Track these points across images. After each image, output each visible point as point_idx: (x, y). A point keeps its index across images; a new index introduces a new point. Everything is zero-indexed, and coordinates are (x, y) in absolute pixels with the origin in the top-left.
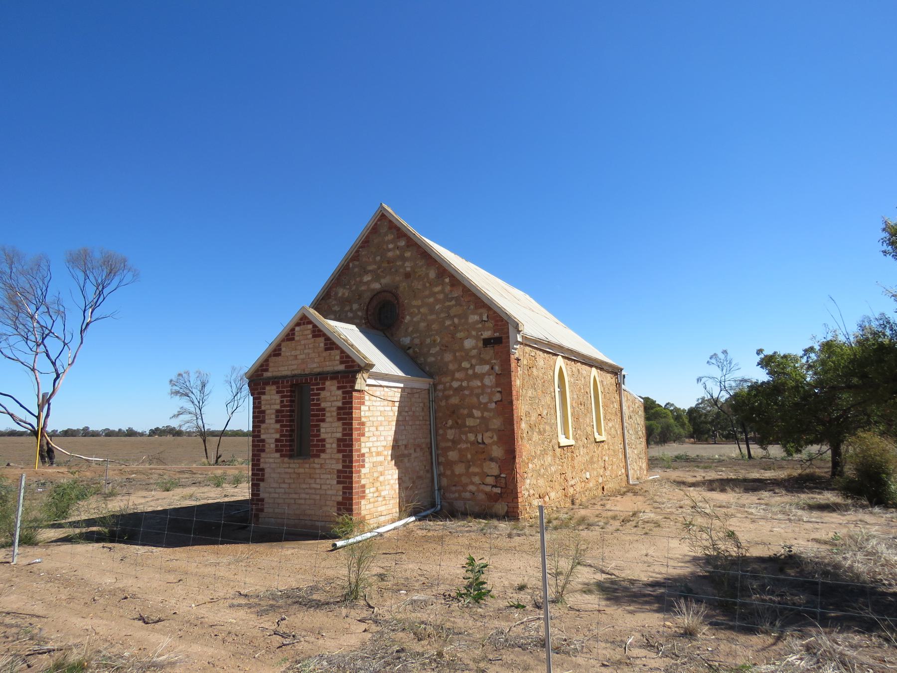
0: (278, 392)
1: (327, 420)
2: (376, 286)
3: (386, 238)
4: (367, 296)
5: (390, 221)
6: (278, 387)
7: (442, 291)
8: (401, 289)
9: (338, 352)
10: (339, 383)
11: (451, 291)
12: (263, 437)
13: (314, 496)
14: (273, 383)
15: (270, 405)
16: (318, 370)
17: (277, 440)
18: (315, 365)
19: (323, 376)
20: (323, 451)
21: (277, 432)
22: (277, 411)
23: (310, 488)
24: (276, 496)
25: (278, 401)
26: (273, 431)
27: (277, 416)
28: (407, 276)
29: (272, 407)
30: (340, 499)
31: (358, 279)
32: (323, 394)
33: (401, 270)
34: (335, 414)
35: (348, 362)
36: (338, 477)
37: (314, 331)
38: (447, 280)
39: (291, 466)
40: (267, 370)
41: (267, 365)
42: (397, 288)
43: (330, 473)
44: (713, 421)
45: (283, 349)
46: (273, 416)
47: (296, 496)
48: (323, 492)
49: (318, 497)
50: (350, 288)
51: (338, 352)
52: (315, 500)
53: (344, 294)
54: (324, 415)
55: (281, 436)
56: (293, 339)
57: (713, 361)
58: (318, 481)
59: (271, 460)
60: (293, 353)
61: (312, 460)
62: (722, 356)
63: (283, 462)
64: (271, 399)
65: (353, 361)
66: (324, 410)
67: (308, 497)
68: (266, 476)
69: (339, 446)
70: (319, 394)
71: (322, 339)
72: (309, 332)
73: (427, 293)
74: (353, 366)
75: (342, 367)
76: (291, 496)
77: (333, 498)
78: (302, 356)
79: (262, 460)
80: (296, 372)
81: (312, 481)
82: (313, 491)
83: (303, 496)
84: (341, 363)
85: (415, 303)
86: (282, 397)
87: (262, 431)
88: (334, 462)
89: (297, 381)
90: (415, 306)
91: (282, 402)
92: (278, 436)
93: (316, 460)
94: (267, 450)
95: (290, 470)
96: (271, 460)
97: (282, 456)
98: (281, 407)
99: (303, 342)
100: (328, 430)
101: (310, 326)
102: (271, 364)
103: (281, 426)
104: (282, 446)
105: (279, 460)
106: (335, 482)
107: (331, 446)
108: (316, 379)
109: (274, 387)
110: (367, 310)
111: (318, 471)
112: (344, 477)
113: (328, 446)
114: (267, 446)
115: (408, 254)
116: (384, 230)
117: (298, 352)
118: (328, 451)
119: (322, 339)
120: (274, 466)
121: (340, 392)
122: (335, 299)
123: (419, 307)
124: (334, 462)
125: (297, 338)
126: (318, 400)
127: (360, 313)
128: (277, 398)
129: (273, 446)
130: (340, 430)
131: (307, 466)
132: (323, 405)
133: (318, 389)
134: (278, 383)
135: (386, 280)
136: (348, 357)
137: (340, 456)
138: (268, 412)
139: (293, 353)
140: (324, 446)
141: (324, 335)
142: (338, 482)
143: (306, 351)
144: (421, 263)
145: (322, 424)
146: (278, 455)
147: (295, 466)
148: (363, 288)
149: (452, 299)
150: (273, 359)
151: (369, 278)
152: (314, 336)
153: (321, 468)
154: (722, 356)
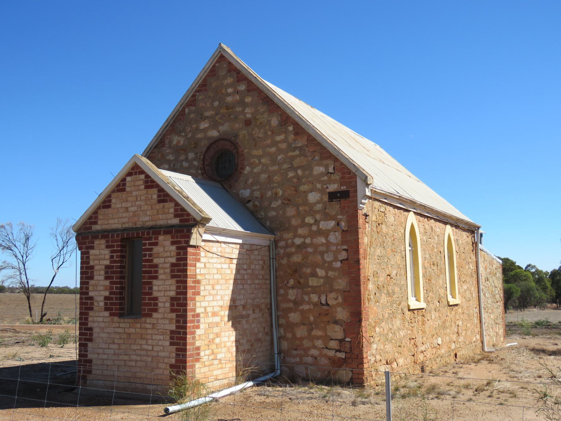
0: (107, 247)
1: (161, 277)
2: (214, 134)
3: (226, 82)
4: (204, 144)
6: (107, 242)
7: (285, 141)
10: (172, 237)
11: (295, 140)
13: (145, 358)
14: (103, 237)
16: (151, 224)
17: (106, 298)
18: (147, 218)
20: (156, 310)
21: (106, 290)
22: (107, 267)
23: (141, 350)
24: (105, 357)
25: (108, 257)
26: (102, 288)
27: (106, 273)
28: (248, 123)
29: (102, 262)
30: (173, 361)
34: (168, 271)
36: (172, 338)
37: (146, 182)
38: (291, 128)
39: (121, 325)
40: (96, 223)
41: (96, 218)
42: (236, 136)
43: (163, 334)
45: (114, 201)
46: (102, 272)
47: (126, 358)
48: (155, 354)
49: (149, 359)
50: (186, 136)
51: (172, 204)
53: (179, 142)
54: (156, 272)
55: (111, 293)
56: (124, 190)
58: (150, 342)
59: (100, 319)
60: (124, 205)
63: (113, 322)
64: (100, 254)
65: (189, 215)
66: (156, 266)
67: (139, 358)
68: (95, 335)
70: (151, 250)
71: (155, 190)
72: (141, 182)
73: (269, 142)
74: (188, 220)
75: (176, 221)
76: (121, 357)
77: (166, 360)
80: (127, 226)
81: (144, 342)
82: (144, 353)
84: (176, 216)
85: (255, 152)
86: (112, 252)
87: (91, 288)
88: (167, 322)
89: (128, 234)
90: (255, 156)
91: (112, 257)
92: (107, 293)
93: (148, 320)
94: (95, 308)
95: (120, 330)
96: (100, 319)
97: (111, 315)
98: (111, 262)
99: (134, 193)
100: (161, 288)
101: (142, 177)
106: (168, 343)
107: (164, 305)
109: (103, 241)
111: (149, 332)
115: (248, 100)
116: (222, 73)
119: (155, 190)
120: (102, 325)
122: (170, 147)
123: (259, 157)
125: (128, 189)
126: (150, 255)
127: (196, 163)
128: (107, 253)
129: (102, 304)
130: (174, 288)
131: (138, 326)
133: (150, 244)
135: (225, 128)
136: (183, 209)
137: (174, 315)
138: (96, 268)
139: (124, 205)
140: (156, 305)
141: (158, 186)
142: (172, 344)
143: (138, 203)
144: (262, 109)
145: (155, 282)
146: (107, 314)
147: (125, 325)
148: (200, 136)
149: (296, 148)
150: (102, 211)
153: (153, 328)
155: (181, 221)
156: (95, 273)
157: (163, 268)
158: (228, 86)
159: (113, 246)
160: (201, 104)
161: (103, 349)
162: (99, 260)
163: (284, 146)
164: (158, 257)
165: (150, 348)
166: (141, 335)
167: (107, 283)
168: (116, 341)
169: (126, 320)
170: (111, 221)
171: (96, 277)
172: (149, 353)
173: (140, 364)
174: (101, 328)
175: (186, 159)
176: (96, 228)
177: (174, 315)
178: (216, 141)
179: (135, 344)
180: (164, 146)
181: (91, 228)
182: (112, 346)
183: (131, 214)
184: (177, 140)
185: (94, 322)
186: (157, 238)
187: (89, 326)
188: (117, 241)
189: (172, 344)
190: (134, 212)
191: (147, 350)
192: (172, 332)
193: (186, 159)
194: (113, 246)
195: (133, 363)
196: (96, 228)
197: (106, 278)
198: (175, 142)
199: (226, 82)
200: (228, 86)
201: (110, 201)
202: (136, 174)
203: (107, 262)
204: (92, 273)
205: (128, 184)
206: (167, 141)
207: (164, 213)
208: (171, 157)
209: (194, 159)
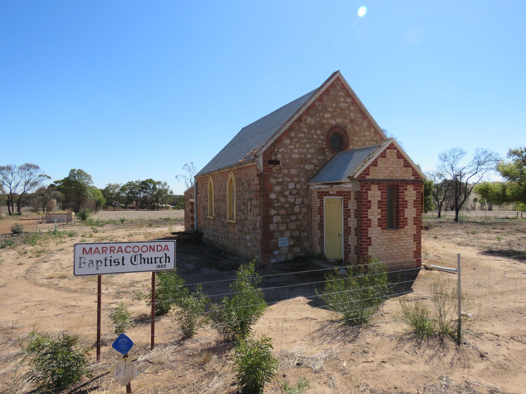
0: (379, 190)
1: (409, 207)
2: (333, 122)
3: (340, 94)
4: (327, 127)
5: (342, 84)
6: (379, 187)
7: (370, 135)
8: (348, 128)
9: (411, 169)
10: (414, 186)
11: (374, 136)
12: (369, 218)
13: (401, 250)
14: (378, 184)
15: (374, 197)
16: (400, 178)
17: (379, 220)
18: (399, 175)
19: (407, 182)
20: (406, 225)
21: (379, 215)
22: (379, 201)
23: (399, 246)
24: (379, 253)
25: (380, 195)
26: (376, 214)
27: (379, 205)
28: (352, 121)
29: (376, 198)
30: (415, 249)
31: (321, 114)
32: (406, 192)
33: (348, 116)
34: (412, 204)
35: (416, 175)
36: (414, 238)
37: (398, 154)
38: (373, 130)
39: (388, 234)
40: (368, 174)
41: (368, 171)
42: (346, 127)
43: (410, 236)
44: (115, 197)
45: (379, 162)
46: (376, 205)
47: (391, 251)
48: (406, 247)
49: (404, 250)
50: (315, 119)
51: (411, 169)
52: (402, 252)
53: (311, 122)
54: (407, 204)
55: (382, 217)
56: (385, 157)
57: (186, 167)
58: (403, 241)
59: (376, 232)
60: (385, 165)
61: (400, 230)
62: (191, 166)
63: (383, 233)
64: (375, 194)
65: (419, 175)
66: (406, 201)
67: (398, 251)
68: (373, 242)
69: (414, 221)
70: (404, 192)
71: (402, 160)
72: (395, 154)
73: (362, 134)
74: (418, 178)
75: (413, 178)
76: (388, 252)
77: (412, 250)
78: (391, 169)
79: (369, 232)
80: (387, 178)
81: (401, 242)
82: (401, 247)
83: (395, 251)
84: (413, 175)
85: (355, 138)
86: (382, 193)
87: (369, 214)
88: (412, 230)
89: (392, 183)
90: (355, 140)
91: (382, 196)
92: (379, 217)
93: (403, 230)
94: (372, 226)
95: (387, 237)
96: (376, 232)
97: (382, 229)
98: (382, 199)
99: (391, 160)
100: (409, 213)
101: (396, 151)
102: (371, 171)
103: (382, 211)
104: (382, 223)
105: (380, 232)
106: (412, 241)
107: (410, 221)
108: (403, 184)
109: (377, 186)
110: (327, 136)
111: (403, 236)
112: (417, 238)
113: (408, 221)
114: (372, 223)
115: (352, 108)
116: (339, 88)
117: (388, 166)
118: (409, 224)
119: (402, 160)
120: (377, 235)
121: (415, 192)
122: (305, 124)
123: (357, 141)
124: (412, 230)
125: (387, 157)
126: (403, 195)
127: (322, 137)
128: (379, 193)
129: (376, 223)
130: (415, 212)
131: (398, 233)
132: (406, 199)
133: (403, 189)
134: (380, 183)
135: (339, 120)
136: (416, 172)
137: (415, 226)
138: (373, 202)
139: (385, 165)
140: (406, 222)
141: (403, 158)
142: (414, 241)
143: (393, 166)
144: (359, 115)
145: (406, 210)
146: (380, 228)
147: (390, 234)
148: (325, 121)
149: (374, 140)
150: (372, 168)
151: (329, 116)
152: (398, 157)
153: (405, 234)
154: (191, 166)
155: (415, 178)
156: (372, 205)
157: (410, 203)
158: (341, 97)
159: (382, 189)
160: (325, 103)
161: (378, 249)
162: (374, 197)
163: (369, 138)
164: (407, 197)
165: (404, 244)
166: (399, 238)
167: (380, 211)
168: (385, 243)
169: (391, 231)
170: (377, 175)
171: (372, 208)
172: (403, 247)
173: (398, 254)
174: (376, 237)
175: (316, 134)
176: (368, 177)
177: (415, 226)
178: (334, 128)
179: (396, 243)
180: (301, 122)
181: (365, 177)
182: (383, 246)
183: (390, 171)
184: (309, 120)
185: (372, 234)
186: (406, 186)
187: (369, 236)
188: (385, 186)
189: (414, 241)
190: (392, 170)
191: (402, 246)
192: (414, 235)
193: (316, 134)
194: (382, 189)
195: (395, 254)
196: (368, 177)
197: (379, 208)
198: (309, 121)
199: (340, 94)
200: (341, 97)
201: (377, 162)
202: (392, 149)
203: (380, 199)
204: (370, 205)
205: (387, 154)
206: (303, 120)
207: (407, 173)
208: (306, 130)
209: (321, 135)
